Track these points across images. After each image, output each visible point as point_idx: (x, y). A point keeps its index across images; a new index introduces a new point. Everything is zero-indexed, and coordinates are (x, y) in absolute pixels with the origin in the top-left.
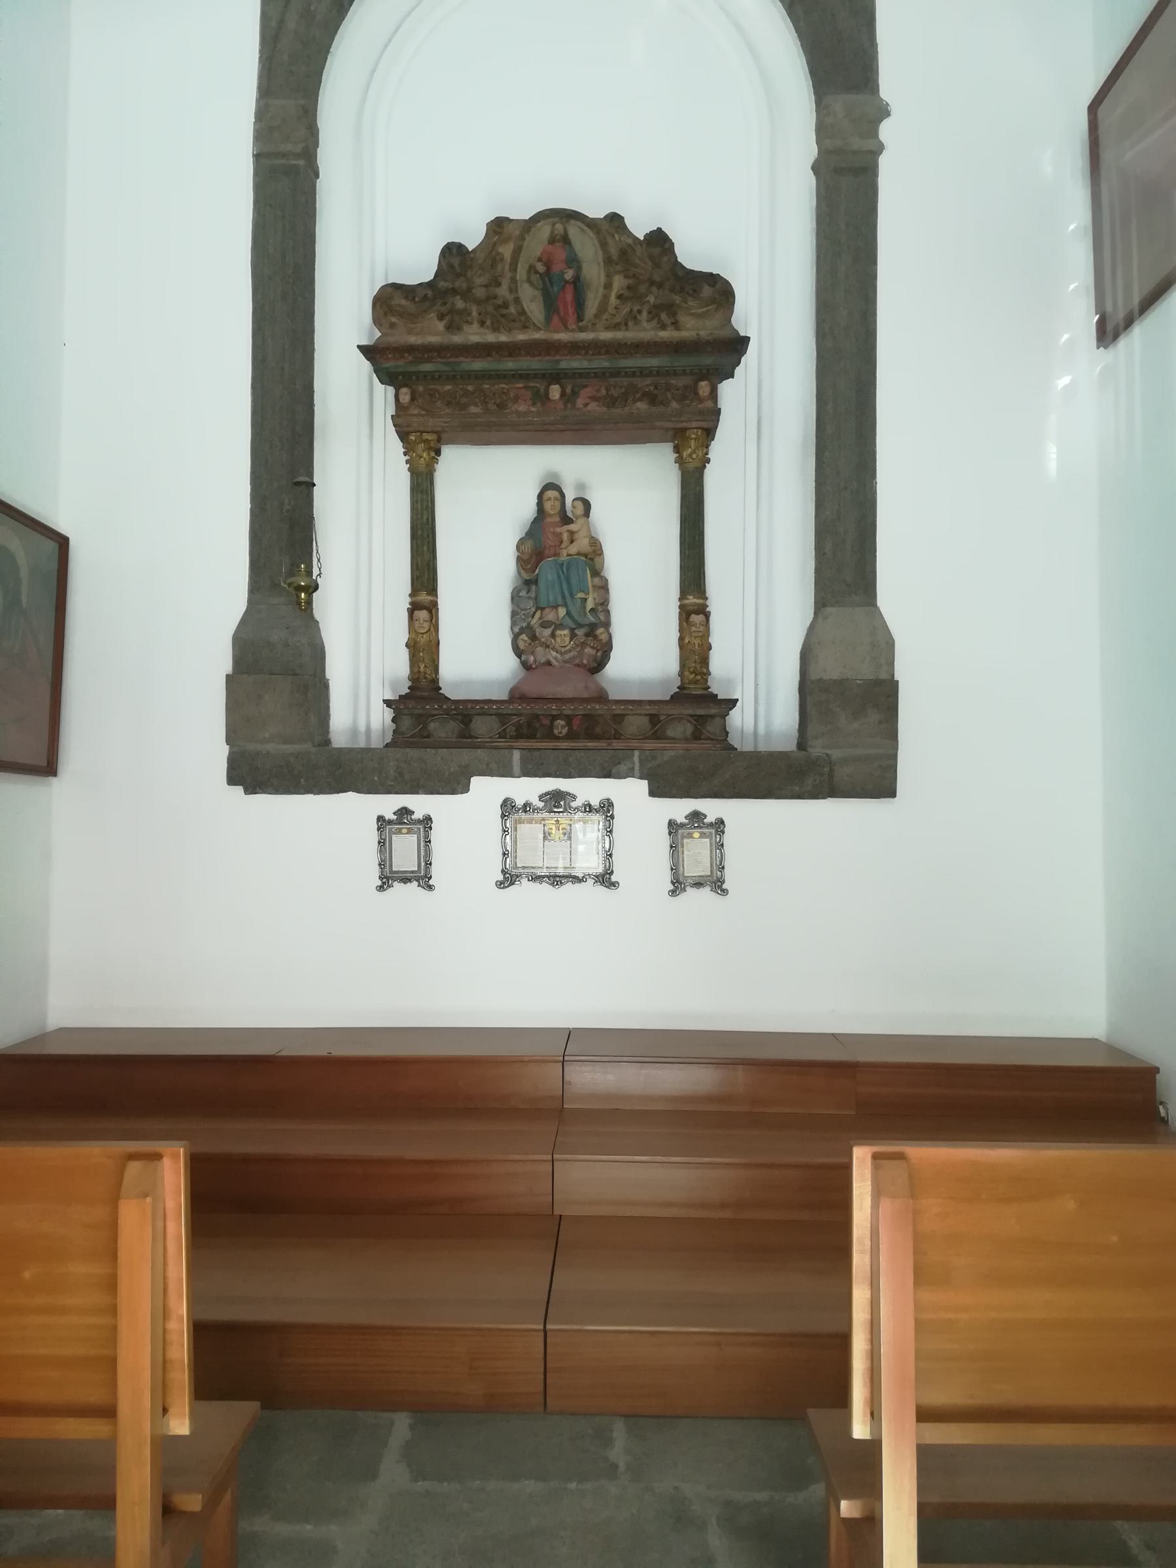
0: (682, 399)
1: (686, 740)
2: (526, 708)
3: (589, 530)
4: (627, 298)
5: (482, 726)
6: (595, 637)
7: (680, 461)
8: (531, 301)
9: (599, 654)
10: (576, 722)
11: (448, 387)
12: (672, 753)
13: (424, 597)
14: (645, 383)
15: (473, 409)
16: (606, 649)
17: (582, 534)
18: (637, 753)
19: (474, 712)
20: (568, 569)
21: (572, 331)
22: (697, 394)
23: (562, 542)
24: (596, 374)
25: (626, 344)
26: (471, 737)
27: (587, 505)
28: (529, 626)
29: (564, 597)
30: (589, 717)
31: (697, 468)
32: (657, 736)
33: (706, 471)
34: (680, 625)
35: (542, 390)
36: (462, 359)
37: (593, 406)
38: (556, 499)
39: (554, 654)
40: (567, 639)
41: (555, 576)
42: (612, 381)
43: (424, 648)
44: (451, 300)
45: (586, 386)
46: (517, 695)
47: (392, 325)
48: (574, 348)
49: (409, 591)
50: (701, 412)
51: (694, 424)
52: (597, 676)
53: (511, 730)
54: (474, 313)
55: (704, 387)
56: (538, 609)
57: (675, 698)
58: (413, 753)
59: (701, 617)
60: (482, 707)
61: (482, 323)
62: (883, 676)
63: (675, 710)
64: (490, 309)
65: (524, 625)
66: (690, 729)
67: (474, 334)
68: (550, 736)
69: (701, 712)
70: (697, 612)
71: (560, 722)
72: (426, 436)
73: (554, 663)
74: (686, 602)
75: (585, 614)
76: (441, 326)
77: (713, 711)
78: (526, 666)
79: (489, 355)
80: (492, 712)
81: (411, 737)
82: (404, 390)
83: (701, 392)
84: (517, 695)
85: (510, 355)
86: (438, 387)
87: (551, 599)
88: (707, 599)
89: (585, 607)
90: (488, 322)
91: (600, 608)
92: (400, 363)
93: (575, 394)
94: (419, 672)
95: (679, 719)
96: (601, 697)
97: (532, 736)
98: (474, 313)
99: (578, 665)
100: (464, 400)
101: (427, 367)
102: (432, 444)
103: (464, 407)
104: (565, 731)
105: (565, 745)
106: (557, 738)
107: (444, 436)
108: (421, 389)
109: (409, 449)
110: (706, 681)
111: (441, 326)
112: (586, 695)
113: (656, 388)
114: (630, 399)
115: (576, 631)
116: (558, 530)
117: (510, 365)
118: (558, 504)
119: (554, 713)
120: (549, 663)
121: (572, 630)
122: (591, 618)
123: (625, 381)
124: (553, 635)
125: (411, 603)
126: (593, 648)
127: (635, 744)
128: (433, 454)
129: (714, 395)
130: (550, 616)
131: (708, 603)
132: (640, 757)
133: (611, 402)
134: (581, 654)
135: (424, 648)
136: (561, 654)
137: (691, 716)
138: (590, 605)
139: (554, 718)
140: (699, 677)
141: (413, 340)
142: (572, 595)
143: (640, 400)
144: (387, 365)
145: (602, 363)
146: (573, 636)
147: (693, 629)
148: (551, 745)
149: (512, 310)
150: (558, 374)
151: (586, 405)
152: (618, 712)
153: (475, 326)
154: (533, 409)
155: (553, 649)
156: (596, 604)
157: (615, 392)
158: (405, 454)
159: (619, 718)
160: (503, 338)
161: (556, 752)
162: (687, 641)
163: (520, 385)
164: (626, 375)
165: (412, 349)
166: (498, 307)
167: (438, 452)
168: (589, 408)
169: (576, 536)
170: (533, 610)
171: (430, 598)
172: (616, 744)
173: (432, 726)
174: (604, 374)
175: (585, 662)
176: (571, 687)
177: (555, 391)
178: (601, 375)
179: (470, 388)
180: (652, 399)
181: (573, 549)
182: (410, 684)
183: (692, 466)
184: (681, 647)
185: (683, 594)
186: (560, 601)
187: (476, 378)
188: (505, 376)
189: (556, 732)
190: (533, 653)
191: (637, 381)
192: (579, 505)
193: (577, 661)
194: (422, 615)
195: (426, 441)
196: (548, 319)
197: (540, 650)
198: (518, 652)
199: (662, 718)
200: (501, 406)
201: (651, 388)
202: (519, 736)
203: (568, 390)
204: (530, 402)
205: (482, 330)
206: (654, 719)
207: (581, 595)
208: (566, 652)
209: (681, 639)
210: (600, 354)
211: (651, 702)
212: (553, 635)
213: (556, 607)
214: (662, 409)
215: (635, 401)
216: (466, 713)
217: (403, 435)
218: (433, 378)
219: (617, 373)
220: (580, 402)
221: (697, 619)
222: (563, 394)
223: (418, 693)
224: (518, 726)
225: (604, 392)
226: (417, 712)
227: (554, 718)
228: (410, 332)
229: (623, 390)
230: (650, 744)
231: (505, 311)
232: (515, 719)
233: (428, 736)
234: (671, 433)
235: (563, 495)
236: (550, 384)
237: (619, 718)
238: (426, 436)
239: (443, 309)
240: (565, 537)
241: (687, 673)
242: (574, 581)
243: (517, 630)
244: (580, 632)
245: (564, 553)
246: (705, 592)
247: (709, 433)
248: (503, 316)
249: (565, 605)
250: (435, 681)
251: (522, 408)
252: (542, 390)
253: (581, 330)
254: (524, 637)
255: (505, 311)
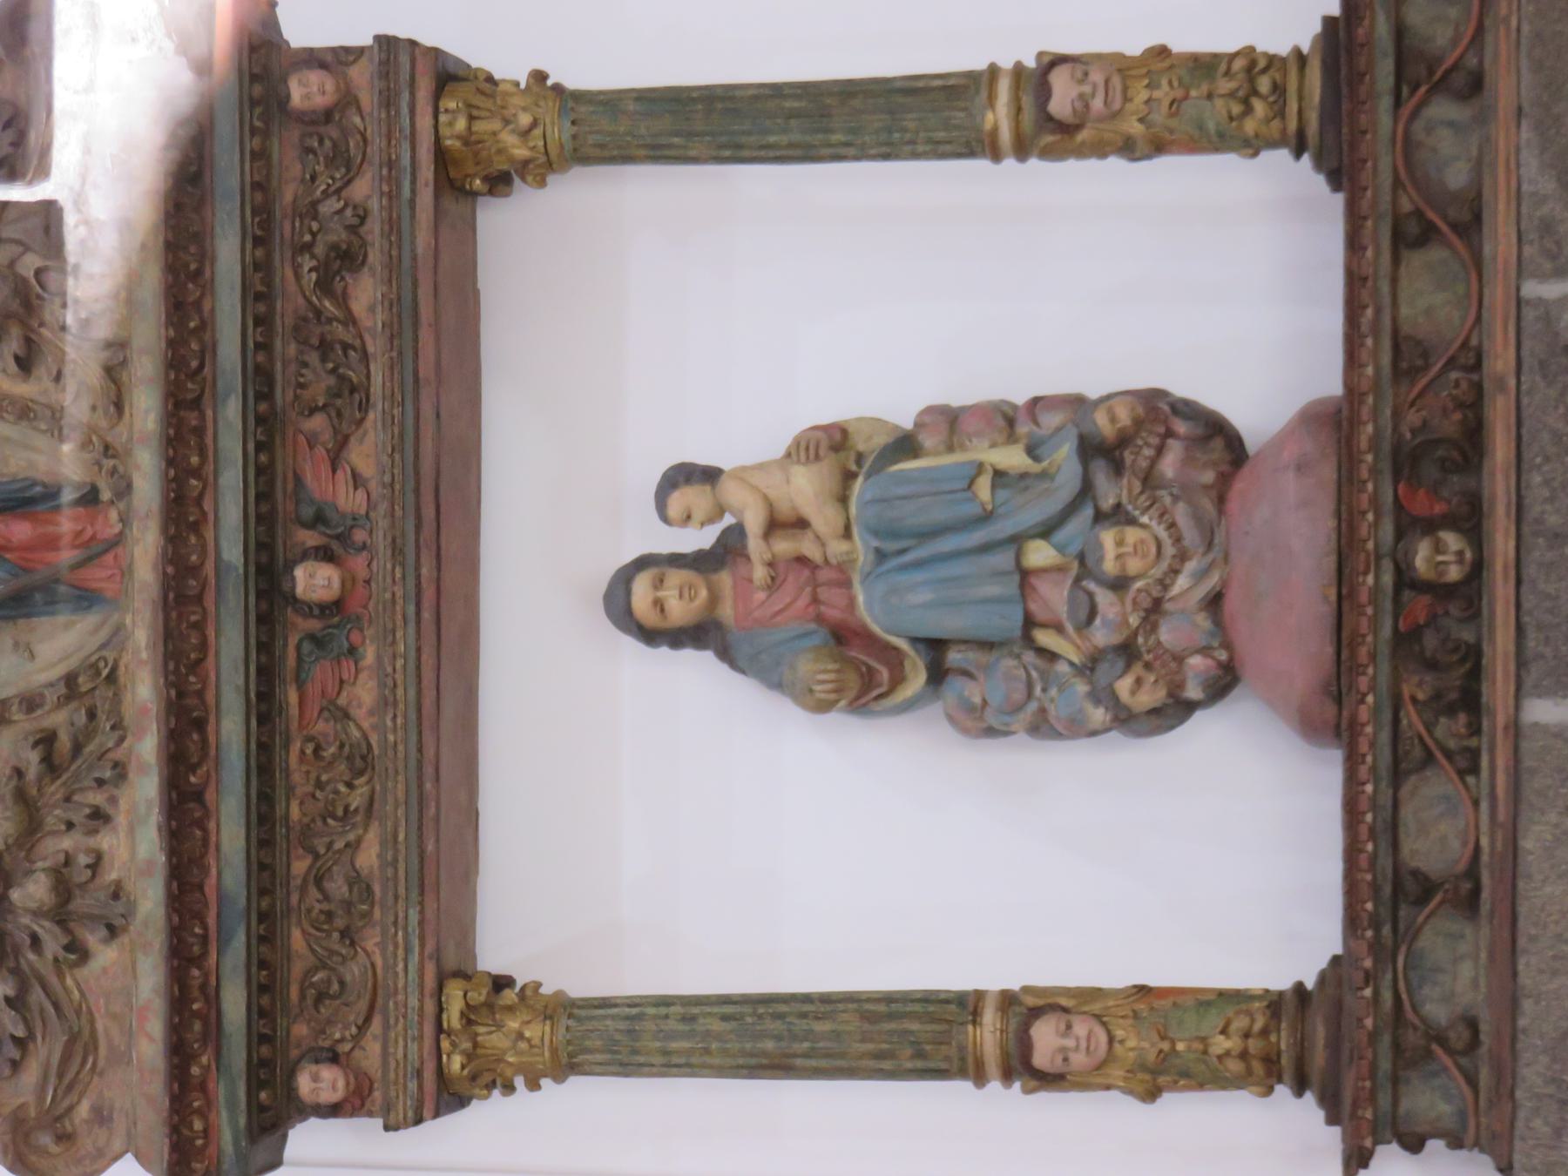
0: (345, 163)
1: (1483, 119)
2: (1375, 677)
3: (761, 467)
4: (29, 342)
5: (1437, 833)
6: (1124, 440)
7: (540, 169)
8: (32, 656)
9: (1181, 427)
10: (1421, 505)
11: (297, 939)
12: (1531, 163)
13: (988, 1034)
14: (295, 284)
15: (368, 858)
16: (1159, 412)
17: (774, 486)
18: (1531, 289)
19: (1386, 862)
20: (895, 535)
21: (124, 520)
22: (328, 115)
23: (801, 560)
24: (259, 447)
25: (171, 343)
26: (1472, 872)
27: (683, 476)
28: (1089, 666)
29: (985, 548)
30: (1406, 462)
31: (562, 111)
32: (1470, 225)
33: (572, 82)
34: (1081, 152)
35: (314, 625)
36: (211, 882)
37: (366, 453)
38: (659, 583)
39: (1182, 582)
40: (1132, 535)
41: (918, 576)
42: (283, 395)
43: (1161, 1043)
44: (26, 920)
45: (298, 480)
46: (1331, 715)
47: (101, 1116)
48: (183, 513)
49: (966, 1086)
50: (388, 101)
51: (425, 122)
52: (1252, 443)
53: (1450, 729)
54: (67, 843)
55: (306, 91)
56: (1028, 640)
57: (1339, 174)
58: (1533, 1072)
59: (1060, 81)
60: (1371, 834)
61: (99, 817)
62: (62, 683)
63: (1383, 165)
64: (55, 790)
65: (1081, 688)
66: (1443, 109)
67: (135, 845)
68: (1469, 591)
69: (1384, 72)
70: (1043, 90)
71: (1422, 558)
72: (453, 1017)
73: (1213, 580)
74: (1006, 136)
75: (1044, 475)
76: (105, 956)
77: (1383, 29)
78: (1223, 684)
79: (198, 796)
80: (1386, 798)
81: (1472, 1082)
82: (304, 1084)
83: (320, 101)
84: (1330, 710)
85: (200, 724)
86: (298, 968)
87: (993, 590)
88: (993, 71)
89: (1024, 476)
90: (97, 798)
91: (1023, 428)
92: (221, 1092)
93: (319, 520)
94: (1244, 1055)
95: (1409, 147)
96: (1334, 423)
97: (1473, 659)
98: (67, 843)
99: (1221, 500)
100: (338, 886)
101: (234, 1004)
102: (479, 996)
103: (357, 880)
104: (1452, 541)
105: (1502, 545)
106: (1478, 569)
107: (451, 961)
108: (301, 1030)
109: (488, 1078)
110: (1272, 60)
111: (105, 956)
112: (1328, 472)
113: (307, 248)
114: (339, 331)
115: (1107, 503)
116: (760, 573)
117: (231, 728)
118: (676, 577)
119: (1388, 579)
120: (1214, 602)
121: (1100, 517)
122: (1064, 454)
123: (285, 348)
124: (1119, 584)
125: (1008, 1076)
126: (1160, 450)
127: (1497, 294)
128: (509, 996)
129: (334, 60)
130: (1055, 597)
131: (1006, 63)
132: (1543, 277)
133: (349, 397)
134: (1185, 492)
135: (1161, 1043)
136: (1183, 556)
137: (1398, 102)
138: (1013, 458)
139: (1405, 580)
140: (1264, 84)
141: (150, 1046)
142: (987, 517)
143: (343, 301)
144: (227, 1137)
145: (229, 419)
146: (1118, 516)
147: (1097, 104)
148: (1501, 589)
149: (60, 719)
150: (260, 570)
151: (357, 480)
152: (1386, 359)
153: (105, 841)
154: (369, 655)
155: (1164, 585)
156: (1011, 438)
157: (320, 384)
158: (509, 1088)
159: (1409, 357)
160: (147, 747)
161: (1530, 571)
162: (1135, 128)
163: (293, 697)
164: (264, 346)
165: (179, 1052)
166: (51, 767)
167: (501, 983)
168: (367, 469)
169: (784, 510)
170: (1029, 657)
171: (989, 1016)
172: (1500, 361)
173: (1437, 1011)
174: (260, 420)
175: (1209, 477)
176: (1288, 534)
177: (314, 581)
178: (266, 429)
179: (300, 866)
180: (348, 258)
181: (824, 518)
182: (1282, 1091)
183: (559, 132)
184: (1159, 147)
185: (984, 146)
186: (1004, 559)
187: (266, 843)
188: (264, 748)
189: (1454, 573)
190: (1179, 659)
191: (284, 318)
192: (678, 501)
193: (1208, 505)
194: (1046, 1038)
195: (468, 1020)
196: (86, 599)
197: (1168, 634)
198: (1174, 710)
199: (1406, 206)
200: (361, 761)
201: (307, 263)
202: (1470, 702)
203: (310, 538)
204: (347, 668)
205: (121, 820)
206: (1411, 234)
207: (983, 487)
208: (1178, 540)
209: (1129, 149)
210: (199, 431)
211: (1354, 244)
212: (1119, 584)
213: (1025, 576)
214: (374, 229)
215: (350, 320)
216: (1387, 894)
217: (449, 1097)
218: (263, 989)
219: (260, 381)
220: (348, 500)
221: (1063, 96)
222: (326, 555)
223: (1319, 1058)
224: (1439, 705)
225: (318, 423)
226: (1385, 1065)
227: (1405, 580)
228: (121, 1058)
229: (313, 358)
230: (1500, 241)
231: (64, 742)
232: (1412, 718)
233: (1472, 1024)
234: (451, 204)
235: (643, 563)
236: (292, 599)
237: (1409, 357)
238: (453, 1017)
239: (53, 944)
240: (784, 546)
241: (1250, 126)
242: (940, 513)
243: (1098, 715)
244: (1109, 492)
245: (837, 548)
246: (972, 76)
247: (448, 75)
248: (77, 748)
249: (1017, 541)
250: (1274, 1003)
251: (363, 694)
252: (314, 625)
253: (125, 489)
254: (1124, 686)
255: (64, 742)
